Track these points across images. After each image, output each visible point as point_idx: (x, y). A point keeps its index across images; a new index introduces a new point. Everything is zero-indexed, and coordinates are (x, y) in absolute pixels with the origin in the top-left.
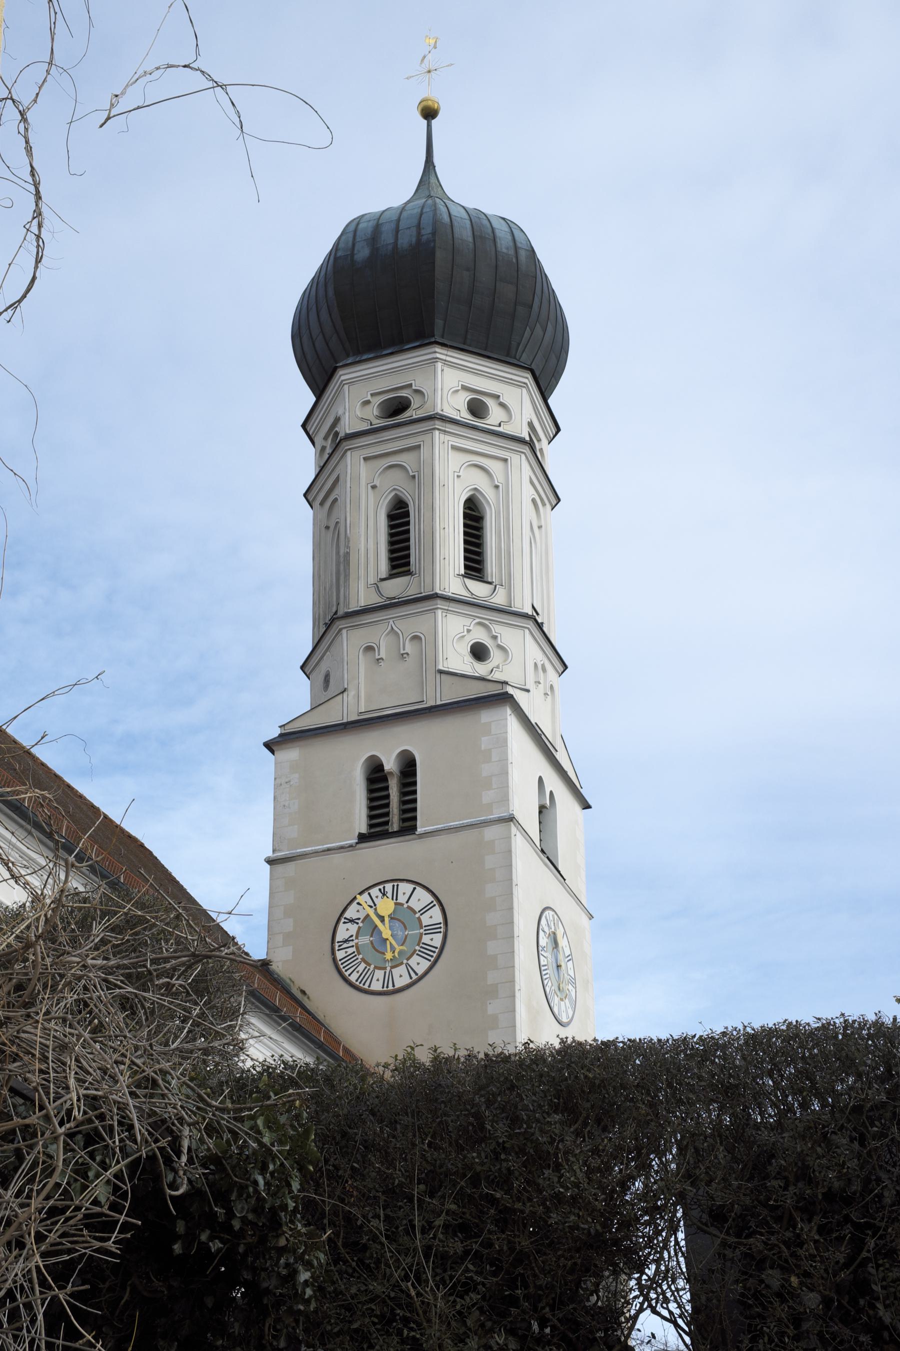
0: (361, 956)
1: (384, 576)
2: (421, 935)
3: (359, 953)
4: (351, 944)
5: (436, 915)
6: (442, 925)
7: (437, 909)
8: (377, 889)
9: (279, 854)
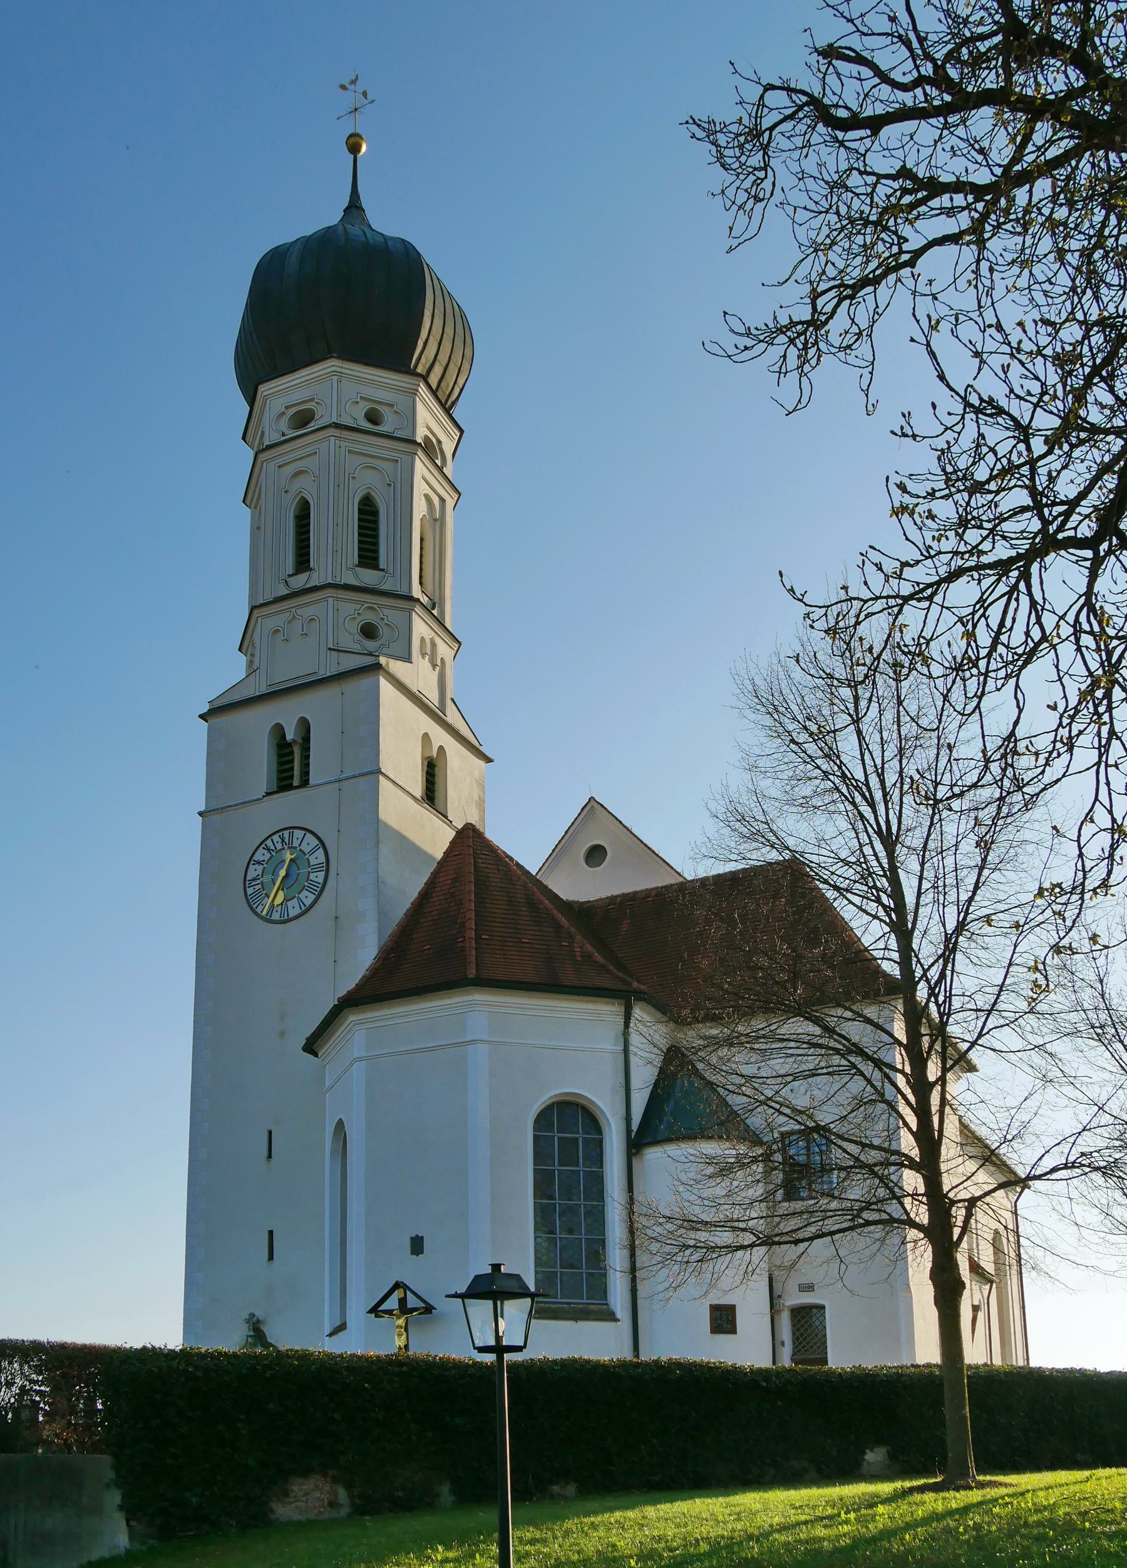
9: (215, 805)
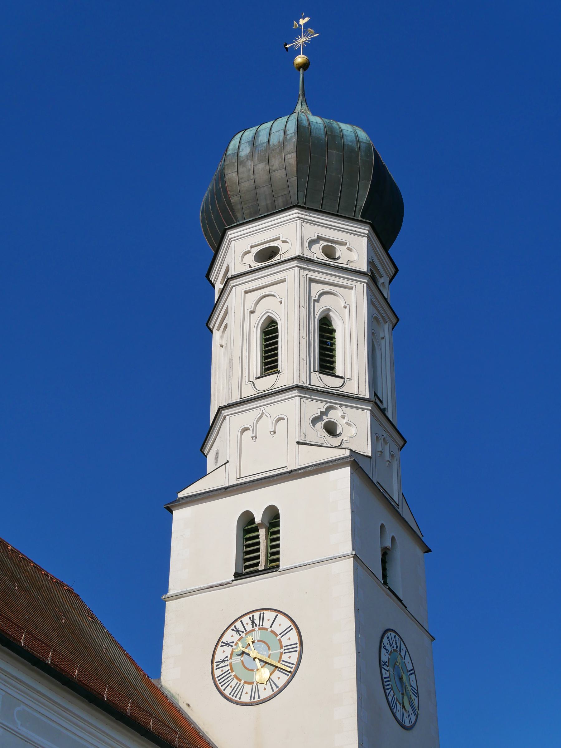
0: (234, 673)
1: (259, 375)
2: (281, 653)
3: (232, 671)
4: (226, 663)
5: (293, 637)
6: (298, 645)
7: (294, 631)
8: (247, 617)
